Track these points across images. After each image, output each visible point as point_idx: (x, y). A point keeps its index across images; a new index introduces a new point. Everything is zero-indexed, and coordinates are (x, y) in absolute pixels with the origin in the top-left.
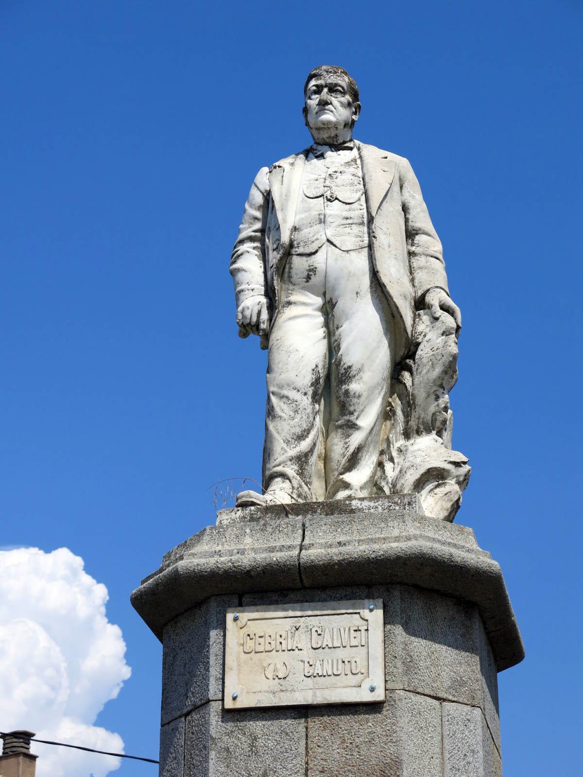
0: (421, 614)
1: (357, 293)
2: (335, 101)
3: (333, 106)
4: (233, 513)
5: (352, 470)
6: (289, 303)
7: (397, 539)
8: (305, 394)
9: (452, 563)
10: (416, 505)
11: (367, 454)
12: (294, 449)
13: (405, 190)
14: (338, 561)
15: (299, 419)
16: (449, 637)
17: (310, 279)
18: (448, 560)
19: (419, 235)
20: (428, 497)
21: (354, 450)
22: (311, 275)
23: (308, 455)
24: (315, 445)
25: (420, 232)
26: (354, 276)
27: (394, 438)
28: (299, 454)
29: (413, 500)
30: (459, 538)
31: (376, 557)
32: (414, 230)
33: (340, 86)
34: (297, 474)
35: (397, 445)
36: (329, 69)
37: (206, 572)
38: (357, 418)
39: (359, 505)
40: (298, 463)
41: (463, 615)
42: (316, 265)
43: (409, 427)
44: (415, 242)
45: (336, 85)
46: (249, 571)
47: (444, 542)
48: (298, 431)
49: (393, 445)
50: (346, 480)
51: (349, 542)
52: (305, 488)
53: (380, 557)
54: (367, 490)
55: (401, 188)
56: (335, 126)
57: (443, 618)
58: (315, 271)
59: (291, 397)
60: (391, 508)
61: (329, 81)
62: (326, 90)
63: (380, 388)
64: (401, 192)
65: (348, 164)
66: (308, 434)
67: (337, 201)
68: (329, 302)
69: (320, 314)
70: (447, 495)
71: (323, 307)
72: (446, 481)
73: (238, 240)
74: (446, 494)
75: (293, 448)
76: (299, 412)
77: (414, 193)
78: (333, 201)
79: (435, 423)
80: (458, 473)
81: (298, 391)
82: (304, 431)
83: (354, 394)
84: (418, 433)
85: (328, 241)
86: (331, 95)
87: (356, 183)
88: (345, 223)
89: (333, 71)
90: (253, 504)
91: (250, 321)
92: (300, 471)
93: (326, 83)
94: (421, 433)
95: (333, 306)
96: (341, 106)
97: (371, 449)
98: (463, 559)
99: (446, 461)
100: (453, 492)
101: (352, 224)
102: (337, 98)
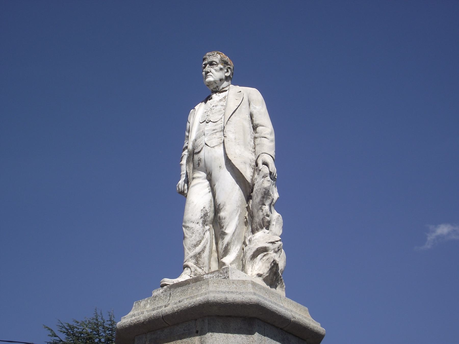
0: (220, 329)
1: (220, 167)
2: (213, 70)
3: (212, 73)
4: (158, 291)
5: (226, 255)
6: (193, 178)
7: (201, 295)
8: (198, 223)
9: (227, 302)
10: (229, 272)
11: (233, 246)
12: (192, 252)
13: (251, 106)
14: (177, 311)
15: (194, 236)
16: (238, 338)
17: (199, 164)
18: (224, 301)
19: (258, 127)
20: (260, 262)
21: (225, 246)
22: (200, 163)
23: (201, 253)
24: (205, 247)
25: (258, 125)
26: (217, 159)
27: (247, 235)
28: (195, 254)
29: (228, 270)
30: (241, 287)
31: (191, 306)
32: (256, 125)
33: (214, 62)
34: (194, 264)
35: (248, 238)
36: (209, 54)
37: (127, 326)
38: (225, 230)
39: (206, 277)
40: (195, 258)
41: (247, 325)
42: (201, 157)
43: (253, 228)
44: (257, 131)
45: (212, 62)
46: (143, 322)
47: (225, 292)
48: (194, 242)
49: (247, 238)
50: (223, 261)
51: (183, 300)
52: (199, 270)
53: (192, 305)
54: (235, 264)
55: (249, 105)
56: (215, 82)
57: (234, 329)
58: (201, 161)
59: (190, 226)
60: (219, 276)
61: (210, 60)
62: (208, 65)
63: (236, 212)
64: (249, 107)
65: (221, 100)
66: (200, 243)
67: (210, 122)
68: (209, 174)
69: (206, 180)
70: (268, 260)
71: (207, 177)
72: (268, 252)
73: (183, 149)
74: (267, 259)
75: (192, 251)
76: (195, 233)
77: (256, 106)
78: (209, 122)
79: (264, 223)
80: (274, 247)
81: (193, 222)
82: (198, 242)
83: (222, 218)
84: (258, 230)
85: (206, 144)
86: (211, 67)
87: (222, 109)
88: (213, 132)
89: (212, 55)
90: (166, 285)
91: (181, 191)
92: (196, 262)
93: (208, 62)
94: (259, 230)
95: (211, 175)
96: (216, 72)
97: (236, 243)
98: (234, 299)
99: (266, 242)
100: (270, 258)
101: (217, 132)
102: (213, 68)
